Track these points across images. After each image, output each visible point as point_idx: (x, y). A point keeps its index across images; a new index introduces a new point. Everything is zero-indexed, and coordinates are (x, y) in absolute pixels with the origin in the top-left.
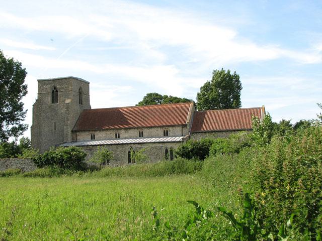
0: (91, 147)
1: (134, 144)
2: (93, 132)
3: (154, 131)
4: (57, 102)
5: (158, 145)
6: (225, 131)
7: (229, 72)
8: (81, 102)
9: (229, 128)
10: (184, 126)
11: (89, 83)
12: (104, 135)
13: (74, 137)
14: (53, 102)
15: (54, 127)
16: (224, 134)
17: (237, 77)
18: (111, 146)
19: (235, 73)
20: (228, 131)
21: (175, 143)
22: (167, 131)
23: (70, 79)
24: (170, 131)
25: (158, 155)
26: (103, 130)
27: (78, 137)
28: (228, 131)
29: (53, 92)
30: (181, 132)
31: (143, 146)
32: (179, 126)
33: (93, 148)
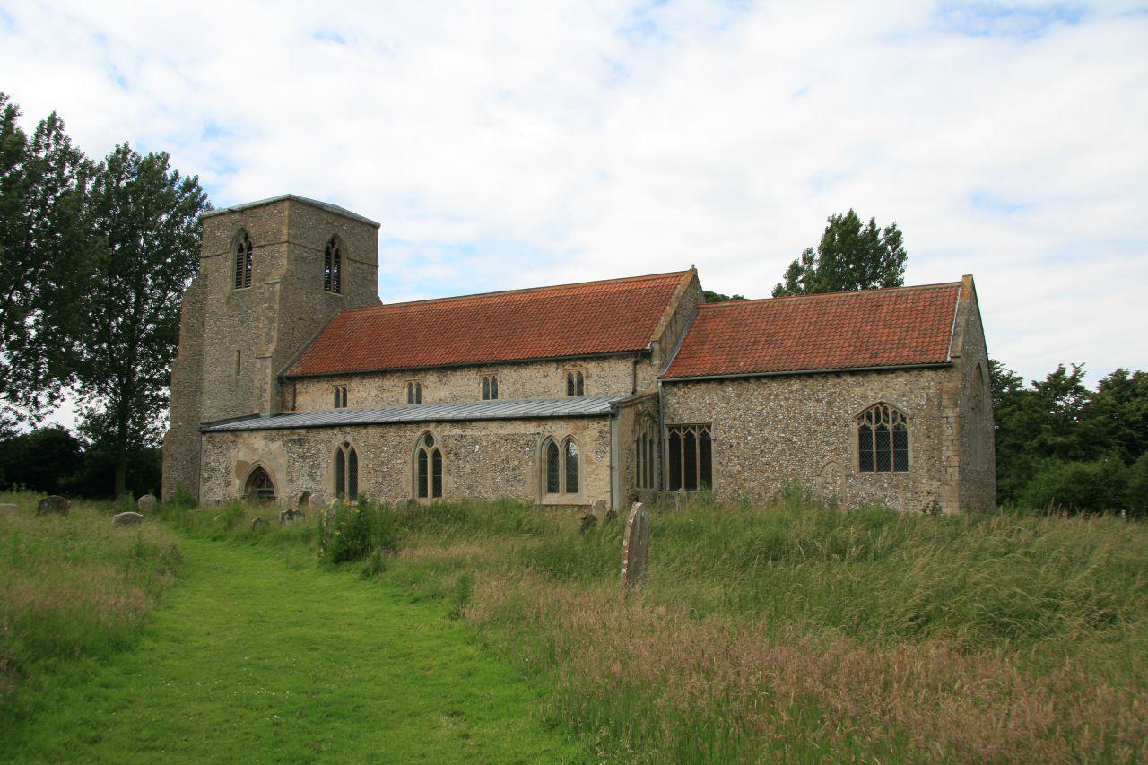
0: (303, 432)
1: (439, 422)
2: (343, 382)
3: (532, 374)
4: (248, 283)
5: (521, 428)
6: (798, 376)
11: (376, 227)
12: (373, 394)
22: (579, 375)
27: (300, 400)
29: (241, 250)
30: (629, 381)
32: (621, 355)
33: (310, 436)
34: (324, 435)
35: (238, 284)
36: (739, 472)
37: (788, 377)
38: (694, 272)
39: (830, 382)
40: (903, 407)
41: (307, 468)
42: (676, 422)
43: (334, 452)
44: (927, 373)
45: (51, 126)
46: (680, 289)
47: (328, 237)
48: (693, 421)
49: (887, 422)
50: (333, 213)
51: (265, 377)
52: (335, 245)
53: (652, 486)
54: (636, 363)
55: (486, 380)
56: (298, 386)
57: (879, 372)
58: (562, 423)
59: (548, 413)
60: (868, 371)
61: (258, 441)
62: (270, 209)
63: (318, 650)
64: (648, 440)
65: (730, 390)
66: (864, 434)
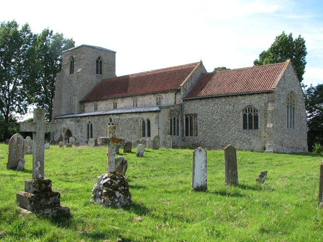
1: (113, 114)
6: (224, 97)
8: (99, 71)
11: (114, 53)
16: (223, 100)
19: (300, 36)
20: (227, 96)
22: (160, 98)
26: (104, 100)
27: (85, 108)
28: (227, 96)
29: (71, 63)
32: (171, 91)
34: (84, 119)
35: (71, 74)
36: (206, 130)
37: (221, 97)
38: (201, 63)
39: (234, 98)
40: (257, 107)
41: (80, 130)
42: (187, 113)
43: (87, 124)
44: (264, 95)
45: (26, 28)
46: (199, 64)
47: (98, 57)
48: (192, 113)
49: (252, 112)
50: (99, 49)
51: (76, 102)
52: (102, 59)
53: (178, 134)
54: (176, 94)
55: (134, 101)
56: (85, 104)
57: (249, 94)
58: (146, 114)
59: (142, 111)
60: (245, 94)
61: (68, 121)
62: (78, 49)
63: (244, 196)
64: (176, 120)
65: (203, 102)
66: (245, 116)
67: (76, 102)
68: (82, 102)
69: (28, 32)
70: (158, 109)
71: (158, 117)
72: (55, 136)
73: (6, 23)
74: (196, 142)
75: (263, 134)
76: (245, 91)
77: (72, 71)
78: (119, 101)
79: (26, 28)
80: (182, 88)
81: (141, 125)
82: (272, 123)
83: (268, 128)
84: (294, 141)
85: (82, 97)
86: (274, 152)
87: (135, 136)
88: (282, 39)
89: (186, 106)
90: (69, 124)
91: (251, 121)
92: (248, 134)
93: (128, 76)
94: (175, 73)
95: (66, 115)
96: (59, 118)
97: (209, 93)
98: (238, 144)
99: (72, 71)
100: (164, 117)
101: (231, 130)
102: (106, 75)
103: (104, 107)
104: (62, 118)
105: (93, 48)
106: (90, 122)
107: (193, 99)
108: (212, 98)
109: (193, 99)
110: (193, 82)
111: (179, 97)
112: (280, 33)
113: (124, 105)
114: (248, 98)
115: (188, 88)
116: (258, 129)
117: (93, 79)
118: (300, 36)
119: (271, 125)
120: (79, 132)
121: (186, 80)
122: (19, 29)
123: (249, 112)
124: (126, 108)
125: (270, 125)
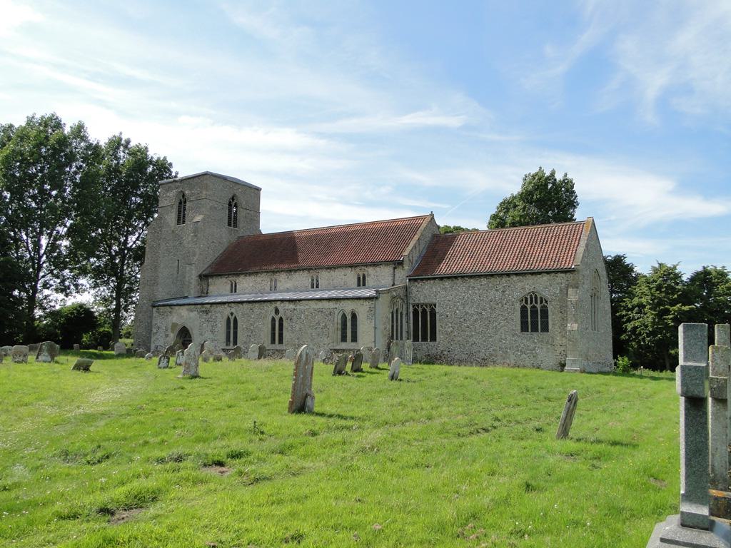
1: (282, 301)
3: (338, 275)
4: (184, 222)
7: (553, 174)
8: (233, 221)
9: (498, 268)
10: (401, 263)
11: (258, 190)
12: (251, 285)
13: (205, 287)
14: (179, 222)
15: (176, 269)
16: (484, 281)
17: (568, 186)
18: (240, 305)
19: (566, 175)
20: (492, 276)
21: (361, 301)
23: (205, 176)
24: (369, 275)
25: (326, 326)
26: (251, 274)
27: (210, 288)
28: (492, 276)
29: (180, 203)
31: (298, 307)
32: (387, 263)
34: (220, 308)
37: (480, 276)
40: (546, 294)
42: (417, 302)
43: (225, 318)
44: (560, 275)
47: (231, 196)
48: (426, 301)
49: (536, 303)
51: (192, 275)
52: (238, 199)
54: (395, 268)
58: (349, 302)
60: (525, 273)
61: (184, 311)
65: (447, 284)
66: (524, 310)
67: (193, 277)
68: (204, 277)
69: (84, 138)
70: (373, 293)
71: (375, 307)
72: (152, 340)
73: (38, 116)
74: (433, 351)
75: (558, 340)
76: (523, 267)
77: (181, 218)
78: (283, 276)
79: (79, 131)
80: (406, 259)
81: (340, 321)
82: (576, 321)
83: (570, 331)
84: (600, 353)
85: (203, 267)
86: (583, 371)
87: (326, 341)
88: (540, 179)
89: (414, 290)
90: (184, 316)
91: (534, 317)
92: (532, 340)
93: (291, 233)
94: (386, 232)
95: (175, 299)
96: (164, 306)
97: (456, 270)
98: (512, 357)
99: (181, 218)
100: (383, 307)
101: (499, 333)
102: (243, 230)
103: (250, 287)
104: (170, 306)
105: (224, 179)
106: (232, 314)
107: (429, 279)
108: (463, 277)
109: (429, 279)
110: (421, 249)
111: (402, 275)
112: (534, 170)
113: (290, 286)
114: (530, 279)
115: (415, 259)
116: (548, 331)
117: (223, 237)
118: (566, 175)
119: (575, 326)
120: (208, 332)
121: (412, 245)
122: (67, 130)
123: (531, 303)
124: (295, 290)
125: (572, 326)
